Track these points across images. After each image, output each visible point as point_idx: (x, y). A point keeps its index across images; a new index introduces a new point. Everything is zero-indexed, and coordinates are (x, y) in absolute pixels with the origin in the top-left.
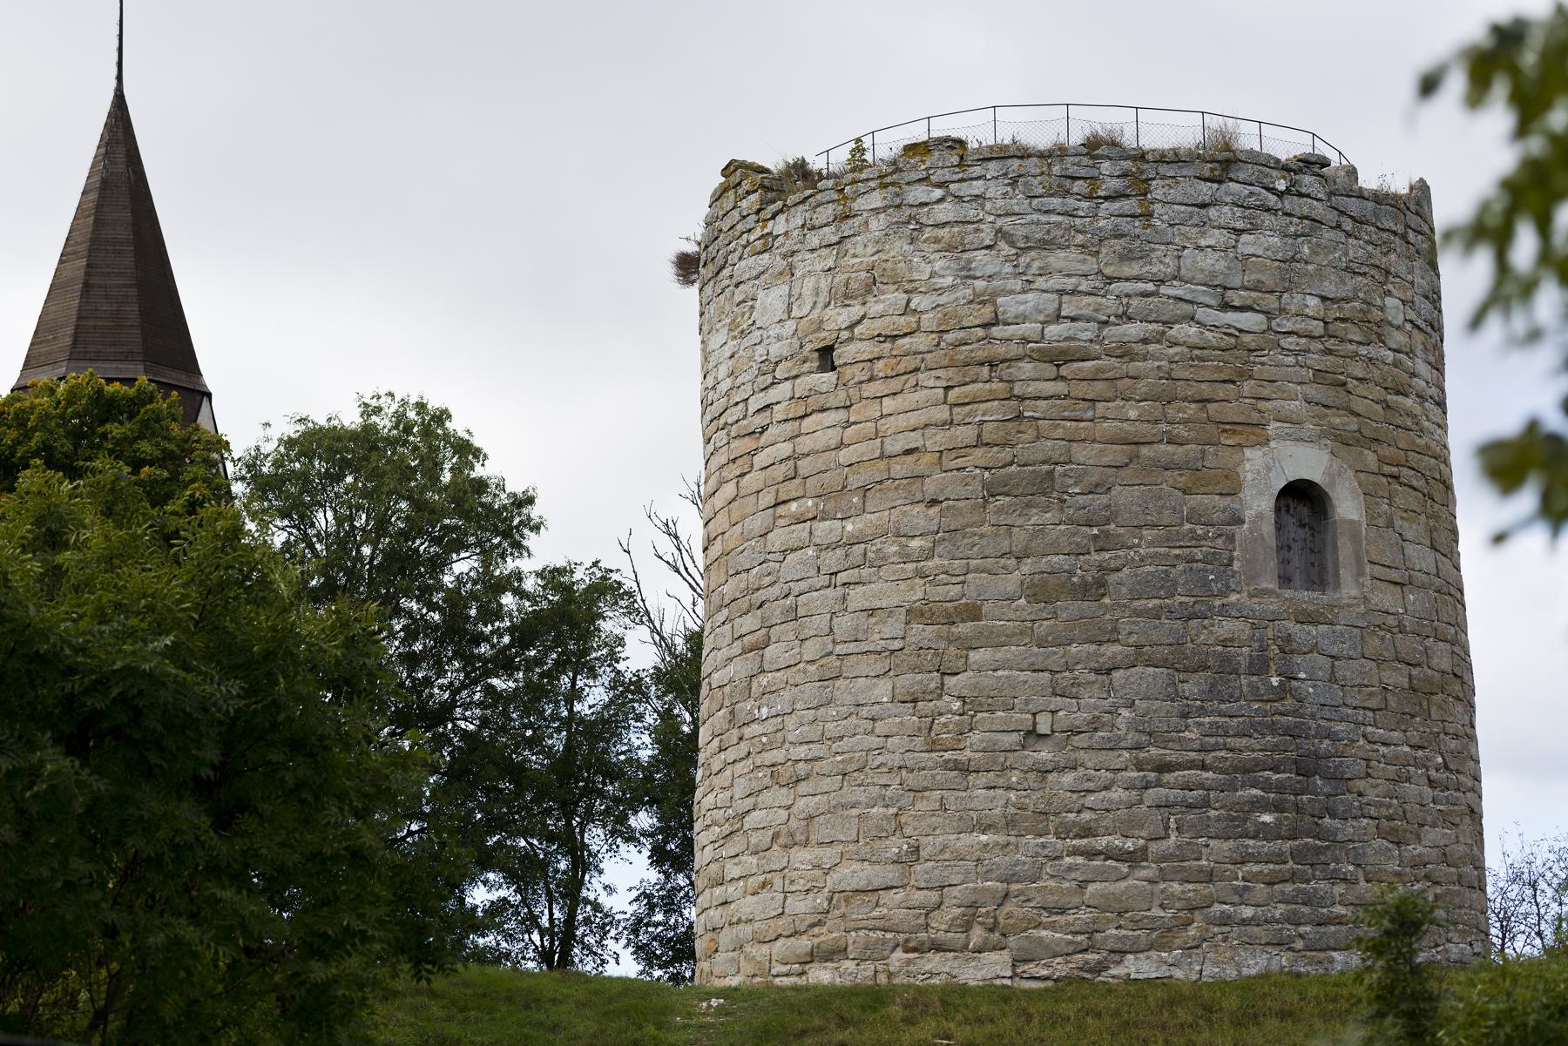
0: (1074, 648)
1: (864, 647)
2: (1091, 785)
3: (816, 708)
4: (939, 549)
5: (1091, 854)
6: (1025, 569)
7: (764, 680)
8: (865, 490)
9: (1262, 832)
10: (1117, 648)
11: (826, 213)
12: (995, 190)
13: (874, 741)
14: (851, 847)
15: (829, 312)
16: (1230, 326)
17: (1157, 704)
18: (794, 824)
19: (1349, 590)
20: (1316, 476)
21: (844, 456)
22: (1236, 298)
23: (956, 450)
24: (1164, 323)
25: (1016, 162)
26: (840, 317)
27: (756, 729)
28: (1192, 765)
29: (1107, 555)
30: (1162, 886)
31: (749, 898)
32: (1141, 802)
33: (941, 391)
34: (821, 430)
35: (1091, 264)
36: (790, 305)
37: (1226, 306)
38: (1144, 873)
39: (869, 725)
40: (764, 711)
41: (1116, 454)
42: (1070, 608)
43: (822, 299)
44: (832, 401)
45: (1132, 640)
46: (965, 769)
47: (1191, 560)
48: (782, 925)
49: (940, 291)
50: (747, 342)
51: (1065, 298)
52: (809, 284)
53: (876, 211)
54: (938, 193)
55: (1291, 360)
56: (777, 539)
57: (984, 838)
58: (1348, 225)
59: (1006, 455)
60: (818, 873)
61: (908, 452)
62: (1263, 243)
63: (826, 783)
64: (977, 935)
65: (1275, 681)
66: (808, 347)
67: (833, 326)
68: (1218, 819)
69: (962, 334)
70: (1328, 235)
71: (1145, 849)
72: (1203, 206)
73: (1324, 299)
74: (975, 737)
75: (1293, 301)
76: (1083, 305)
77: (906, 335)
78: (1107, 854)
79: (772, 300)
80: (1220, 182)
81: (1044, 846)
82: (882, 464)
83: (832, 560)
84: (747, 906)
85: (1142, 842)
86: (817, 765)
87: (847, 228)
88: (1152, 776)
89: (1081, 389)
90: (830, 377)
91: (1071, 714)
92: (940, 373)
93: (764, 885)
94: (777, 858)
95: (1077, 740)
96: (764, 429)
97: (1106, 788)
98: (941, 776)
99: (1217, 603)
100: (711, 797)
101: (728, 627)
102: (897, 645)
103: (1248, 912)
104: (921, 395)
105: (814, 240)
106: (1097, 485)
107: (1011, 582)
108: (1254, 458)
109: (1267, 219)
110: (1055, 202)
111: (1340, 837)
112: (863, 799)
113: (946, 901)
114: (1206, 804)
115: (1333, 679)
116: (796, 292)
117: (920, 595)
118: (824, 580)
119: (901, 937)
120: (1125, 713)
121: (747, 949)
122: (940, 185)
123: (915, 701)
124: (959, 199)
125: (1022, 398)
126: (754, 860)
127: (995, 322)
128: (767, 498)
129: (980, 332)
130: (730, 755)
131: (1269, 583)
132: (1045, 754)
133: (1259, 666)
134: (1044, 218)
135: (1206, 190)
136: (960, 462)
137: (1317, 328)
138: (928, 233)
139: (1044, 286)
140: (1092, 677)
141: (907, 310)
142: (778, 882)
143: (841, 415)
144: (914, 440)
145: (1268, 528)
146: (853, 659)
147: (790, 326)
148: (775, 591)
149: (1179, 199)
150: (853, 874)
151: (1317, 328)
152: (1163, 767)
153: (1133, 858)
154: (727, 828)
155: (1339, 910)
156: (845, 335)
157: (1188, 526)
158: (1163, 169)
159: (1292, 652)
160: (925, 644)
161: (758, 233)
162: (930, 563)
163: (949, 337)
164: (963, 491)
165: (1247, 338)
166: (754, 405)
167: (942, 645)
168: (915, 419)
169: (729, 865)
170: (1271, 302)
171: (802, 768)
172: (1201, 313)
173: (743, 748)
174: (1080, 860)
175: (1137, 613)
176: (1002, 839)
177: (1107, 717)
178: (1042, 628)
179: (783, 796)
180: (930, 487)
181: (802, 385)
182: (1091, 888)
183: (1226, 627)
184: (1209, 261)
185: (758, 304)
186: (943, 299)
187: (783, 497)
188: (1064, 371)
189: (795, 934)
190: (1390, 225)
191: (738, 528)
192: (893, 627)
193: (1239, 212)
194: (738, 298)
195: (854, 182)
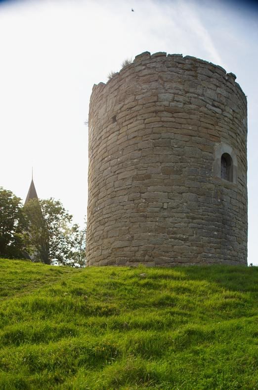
0: (174, 187)
1: (121, 188)
2: (176, 222)
3: (110, 205)
5: (175, 238)
6: (163, 165)
8: (123, 149)
9: (214, 236)
10: (183, 187)
12: (158, 65)
14: (118, 237)
16: (214, 110)
17: (193, 203)
20: (230, 154)
22: (216, 104)
24: (199, 106)
27: (96, 213)
28: (200, 218)
29: (182, 164)
30: (191, 247)
32: (188, 226)
33: (143, 120)
35: (181, 87)
38: (187, 244)
39: (122, 207)
40: (98, 208)
41: (187, 138)
42: (174, 177)
45: (187, 186)
46: (146, 217)
47: (202, 167)
48: (101, 257)
51: (175, 95)
57: (149, 234)
59: (158, 136)
60: (109, 244)
61: (134, 137)
63: (112, 223)
64: (147, 257)
68: (205, 232)
71: (188, 238)
73: (233, 111)
75: (228, 109)
76: (181, 98)
77: (134, 107)
78: (179, 239)
81: (164, 236)
85: (187, 236)
88: (191, 220)
89: (178, 120)
91: (173, 204)
94: (100, 242)
95: (173, 210)
97: (180, 222)
99: (208, 179)
102: (130, 186)
103: (210, 255)
104: (138, 122)
106: (181, 146)
110: (174, 69)
111: (230, 240)
112: (120, 225)
113: (140, 249)
114: (202, 228)
115: (231, 203)
117: (135, 173)
118: (112, 174)
120: (185, 204)
122: (144, 65)
123: (134, 200)
124: (149, 68)
125: (163, 122)
126: (95, 243)
129: (154, 104)
132: (166, 213)
134: (171, 73)
135: (211, 74)
136: (147, 139)
139: (170, 92)
140: (177, 194)
141: (135, 100)
142: (100, 247)
143: (117, 133)
146: (118, 192)
149: (204, 73)
150: (118, 244)
152: (193, 218)
153: (185, 240)
155: (229, 256)
156: (119, 111)
157: (202, 159)
159: (223, 194)
166: (98, 139)
167: (141, 185)
168: (136, 129)
170: (222, 107)
172: (208, 105)
174: (173, 240)
175: (190, 179)
176: (154, 234)
177: (181, 205)
178: (166, 181)
179: (102, 227)
180: (140, 146)
182: (175, 247)
183: (209, 186)
186: (144, 96)
187: (104, 157)
189: (104, 259)
192: (129, 182)
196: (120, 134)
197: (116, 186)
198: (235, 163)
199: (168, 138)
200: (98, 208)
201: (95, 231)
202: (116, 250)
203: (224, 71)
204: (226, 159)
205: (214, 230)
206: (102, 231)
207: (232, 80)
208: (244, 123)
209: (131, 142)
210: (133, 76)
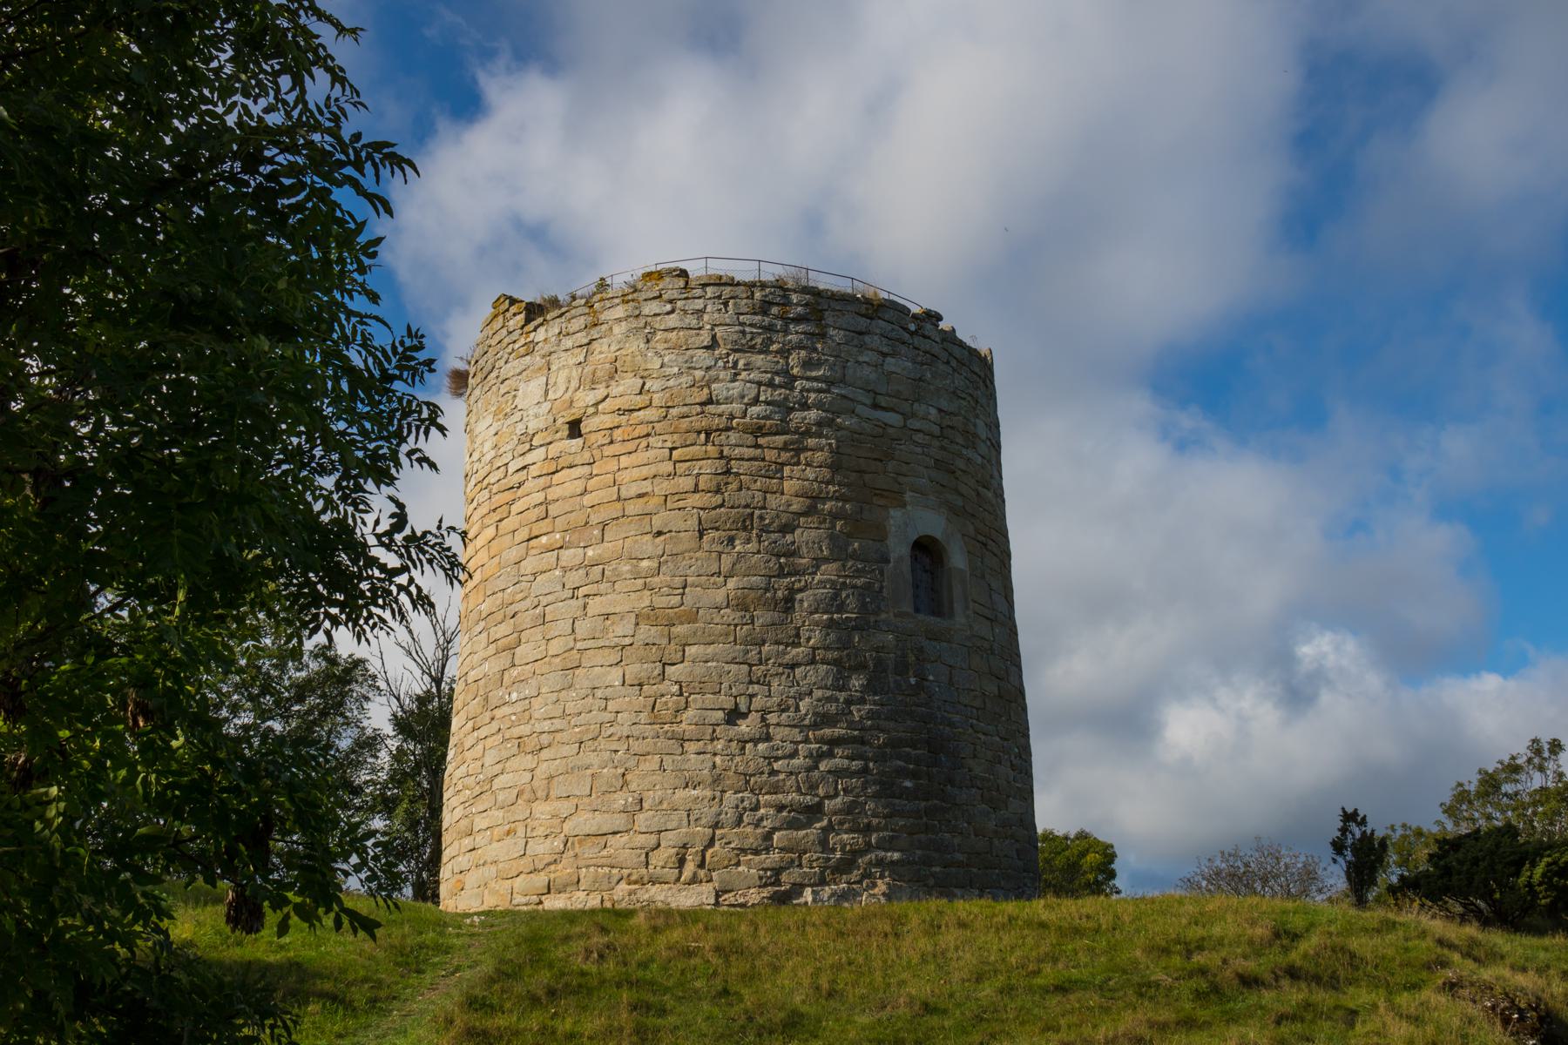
1: (601, 643)
4: (663, 568)
7: (515, 672)
8: (604, 526)
11: (581, 322)
13: (607, 716)
14: (586, 800)
15: (579, 394)
18: (536, 783)
19: (960, 619)
20: (938, 535)
21: (588, 500)
22: (882, 401)
23: (681, 494)
25: (729, 289)
26: (587, 398)
27: (506, 710)
31: (495, 845)
34: (568, 483)
36: (546, 392)
37: (875, 406)
40: (514, 696)
43: (574, 384)
44: (578, 460)
46: (682, 740)
48: (525, 864)
49: (667, 378)
50: (509, 422)
52: (563, 375)
53: (619, 320)
54: (668, 307)
55: (919, 450)
56: (528, 566)
58: (954, 363)
60: (556, 821)
61: (640, 496)
62: (898, 365)
65: (913, 681)
66: (560, 421)
67: (582, 404)
69: (686, 409)
70: (942, 367)
72: (861, 333)
73: (940, 410)
74: (690, 713)
75: (920, 409)
79: (534, 388)
80: (871, 319)
82: (619, 505)
83: (574, 578)
84: (494, 850)
86: (558, 736)
87: (595, 333)
90: (579, 441)
92: (665, 437)
93: (508, 833)
94: (521, 811)
96: (520, 485)
98: (662, 743)
99: (872, 619)
100: (463, 769)
101: (484, 635)
102: (627, 641)
104: (651, 454)
105: (568, 342)
107: (719, 596)
108: (896, 514)
109: (903, 349)
116: (551, 382)
117: (647, 603)
119: (625, 872)
121: (492, 884)
122: (671, 301)
126: (500, 813)
127: (710, 401)
128: (523, 534)
129: (698, 409)
130: (483, 733)
131: (908, 608)
133: (902, 668)
135: (863, 323)
136: (681, 504)
137: (936, 430)
138: (659, 335)
143: (587, 469)
144: (646, 487)
145: (906, 567)
147: (546, 406)
148: (527, 603)
150: (585, 822)
151: (936, 430)
154: (477, 790)
155: (959, 857)
158: (833, 304)
160: (650, 641)
161: (522, 341)
162: (656, 579)
163: (674, 412)
164: (683, 526)
165: (890, 431)
166: (512, 468)
168: (645, 471)
169: (477, 819)
170: (906, 407)
171: (545, 739)
172: (859, 409)
173: (495, 726)
179: (529, 761)
180: (657, 522)
181: (553, 450)
184: (867, 371)
185: (520, 393)
186: (671, 383)
188: (761, 441)
190: (977, 370)
191: (496, 560)
192: (623, 628)
193: (885, 341)
194: (502, 391)
195: (602, 300)
196: (591, 476)
197: (580, 633)
198: (957, 559)
199: (747, 506)
200: (514, 696)
201: (498, 768)
202: (580, 842)
203: (904, 310)
204: (926, 549)
205: (901, 773)
206: (529, 776)
207: (928, 326)
208: (983, 432)
209: (633, 508)
210: (634, 324)
